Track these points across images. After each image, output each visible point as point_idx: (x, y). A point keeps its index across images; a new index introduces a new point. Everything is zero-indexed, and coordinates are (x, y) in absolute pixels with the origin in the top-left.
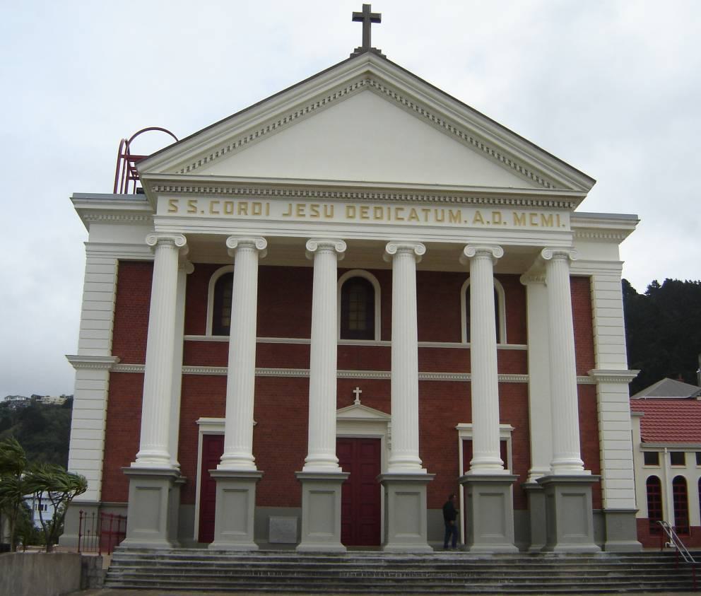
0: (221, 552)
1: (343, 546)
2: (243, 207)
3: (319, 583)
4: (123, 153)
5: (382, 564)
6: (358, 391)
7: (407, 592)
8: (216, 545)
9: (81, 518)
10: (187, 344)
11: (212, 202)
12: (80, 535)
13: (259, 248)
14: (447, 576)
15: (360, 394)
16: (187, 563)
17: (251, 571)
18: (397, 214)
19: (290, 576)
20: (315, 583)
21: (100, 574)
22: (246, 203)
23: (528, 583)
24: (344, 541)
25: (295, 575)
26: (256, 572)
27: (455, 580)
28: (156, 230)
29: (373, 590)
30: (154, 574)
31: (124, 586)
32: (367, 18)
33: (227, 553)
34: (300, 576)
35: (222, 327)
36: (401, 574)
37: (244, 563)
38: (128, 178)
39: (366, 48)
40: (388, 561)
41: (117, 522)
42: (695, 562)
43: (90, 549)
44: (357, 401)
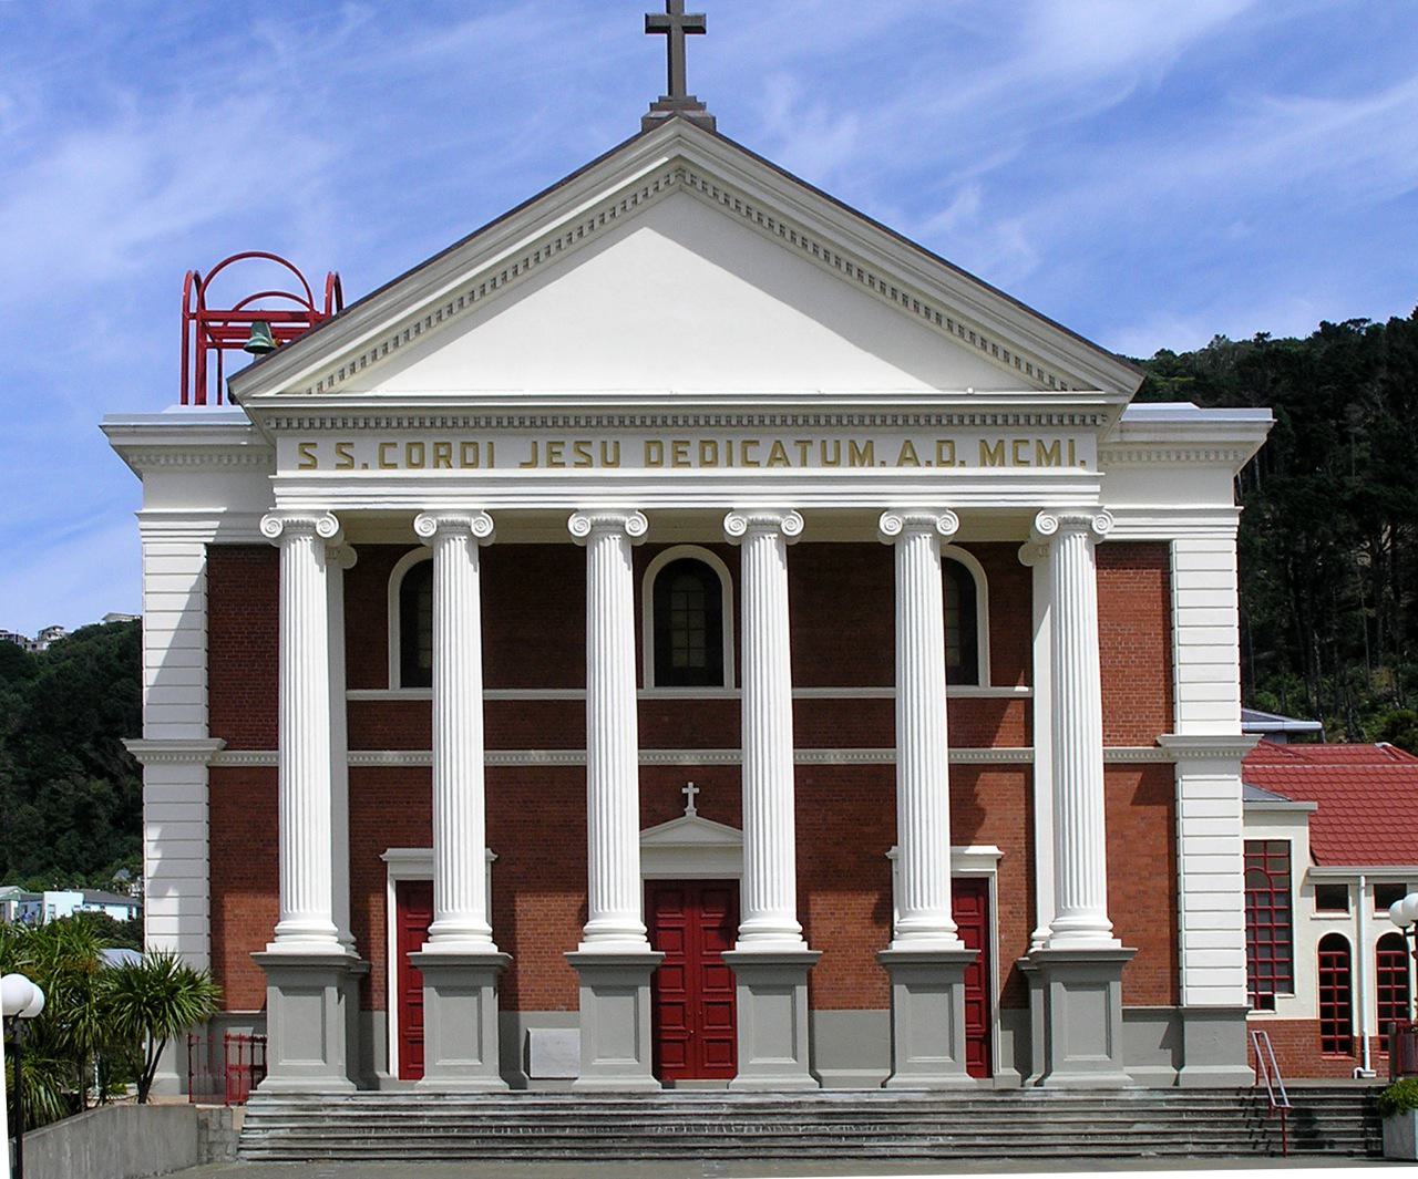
0: (438, 1095)
1: (656, 1081)
2: (443, 451)
3: (608, 1143)
4: (193, 309)
5: (724, 1111)
6: (691, 790)
7: (762, 1157)
8: (428, 1082)
9: (190, 1045)
10: (353, 708)
11: (383, 446)
12: (190, 1075)
13: (476, 533)
14: (836, 1130)
15: (695, 794)
16: (378, 1116)
17: (491, 1127)
18: (745, 453)
19: (558, 1133)
20: (601, 1144)
21: (230, 1137)
22: (449, 444)
23: (979, 1141)
24: (657, 1073)
25: (567, 1132)
26: (498, 1128)
27: (847, 1137)
28: (279, 507)
29: (701, 1153)
30: (323, 1136)
31: (271, 1156)
32: (675, 27)
33: (447, 1097)
34: (575, 1133)
35: (419, 670)
36: (753, 1128)
37: (477, 1113)
38: (202, 350)
39: (676, 103)
40: (734, 1106)
41: (249, 1049)
42: (1288, 1105)
43: (1002, 879)
44: (691, 809)
